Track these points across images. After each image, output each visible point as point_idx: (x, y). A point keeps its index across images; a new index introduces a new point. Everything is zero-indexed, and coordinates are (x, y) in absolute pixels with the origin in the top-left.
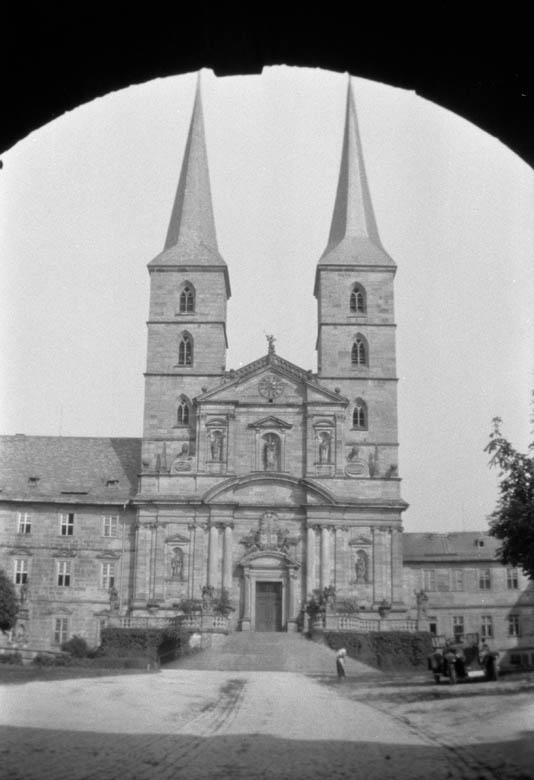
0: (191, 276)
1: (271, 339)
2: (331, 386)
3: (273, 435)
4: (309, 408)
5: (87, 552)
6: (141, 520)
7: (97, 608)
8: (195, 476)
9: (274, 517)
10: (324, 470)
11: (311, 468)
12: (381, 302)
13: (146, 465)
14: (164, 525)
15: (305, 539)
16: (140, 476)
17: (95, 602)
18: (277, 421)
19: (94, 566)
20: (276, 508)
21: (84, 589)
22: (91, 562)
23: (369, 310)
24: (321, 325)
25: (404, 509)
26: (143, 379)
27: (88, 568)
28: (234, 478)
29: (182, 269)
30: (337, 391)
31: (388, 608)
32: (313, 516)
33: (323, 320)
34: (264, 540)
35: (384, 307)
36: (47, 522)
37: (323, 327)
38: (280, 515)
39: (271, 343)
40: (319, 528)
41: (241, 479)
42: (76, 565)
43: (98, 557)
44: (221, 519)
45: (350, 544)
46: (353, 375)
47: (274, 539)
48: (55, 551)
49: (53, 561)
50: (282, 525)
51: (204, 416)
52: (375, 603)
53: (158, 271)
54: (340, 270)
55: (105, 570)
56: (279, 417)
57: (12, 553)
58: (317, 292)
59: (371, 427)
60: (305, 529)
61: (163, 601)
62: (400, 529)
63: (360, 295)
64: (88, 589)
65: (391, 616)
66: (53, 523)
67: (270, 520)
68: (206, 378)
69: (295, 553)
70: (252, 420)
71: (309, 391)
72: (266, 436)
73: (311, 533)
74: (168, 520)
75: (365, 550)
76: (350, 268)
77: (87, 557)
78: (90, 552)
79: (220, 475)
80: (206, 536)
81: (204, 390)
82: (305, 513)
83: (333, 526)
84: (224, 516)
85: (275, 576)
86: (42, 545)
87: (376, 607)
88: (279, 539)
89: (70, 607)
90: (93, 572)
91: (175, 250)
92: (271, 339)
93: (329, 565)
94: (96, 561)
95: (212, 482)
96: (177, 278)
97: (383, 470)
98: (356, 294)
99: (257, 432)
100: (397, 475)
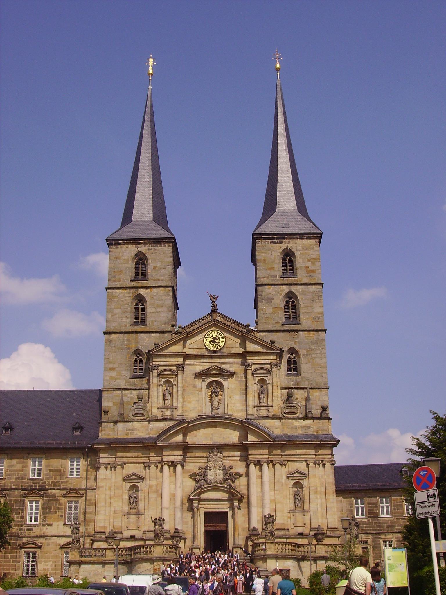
0: (142, 248)
1: (214, 299)
2: (267, 338)
3: (217, 382)
4: (248, 358)
5: (54, 491)
6: (101, 461)
7: (63, 541)
8: (149, 421)
9: (219, 455)
10: (263, 412)
11: (251, 411)
12: (309, 264)
13: (106, 412)
14: (122, 465)
15: (247, 475)
16: (101, 423)
17: (62, 536)
18: (221, 370)
19: (60, 504)
20: (221, 448)
21: (50, 525)
22: (58, 500)
23: (298, 271)
24: (257, 285)
25: (336, 445)
26: (104, 337)
27: (54, 505)
28: (182, 421)
29: (136, 241)
30: (273, 342)
31: (323, 534)
32: (254, 455)
33: (260, 281)
34: (211, 475)
35: (310, 268)
36: (19, 466)
37: (259, 288)
38: (225, 454)
39: (213, 302)
40: (259, 464)
41: (189, 422)
42: (44, 504)
43: (64, 496)
44: (172, 458)
45: (288, 477)
46: (286, 327)
47: (220, 475)
48: (65, 492)
49: (24, 501)
50: (227, 463)
51: (156, 367)
52: (312, 529)
53: (115, 244)
54: (273, 238)
55: (32, 506)
56: (223, 367)
57: (25, 496)
58: (254, 260)
59: (340, 439)
60: (248, 466)
61: (121, 532)
62: (333, 464)
63: (290, 259)
64: (55, 524)
65: (326, 541)
66: (23, 467)
67: (217, 459)
68: (158, 334)
69: (240, 484)
70: (198, 368)
71: (247, 342)
72: (211, 383)
73: (252, 467)
74: (125, 460)
75: (301, 482)
76: (282, 236)
77: (54, 496)
78: (58, 491)
79: (171, 419)
80: (145, 471)
81: (156, 345)
82: (247, 450)
83: (272, 461)
84: (176, 456)
85: (224, 507)
86: (14, 487)
87: (312, 533)
88: (225, 475)
89: (39, 541)
90: (59, 509)
91: (126, 228)
92: (214, 299)
93: (269, 495)
94: (63, 500)
95: (162, 425)
96: (131, 251)
97: (317, 412)
98: (288, 259)
99: (204, 380)
100: (328, 414)
